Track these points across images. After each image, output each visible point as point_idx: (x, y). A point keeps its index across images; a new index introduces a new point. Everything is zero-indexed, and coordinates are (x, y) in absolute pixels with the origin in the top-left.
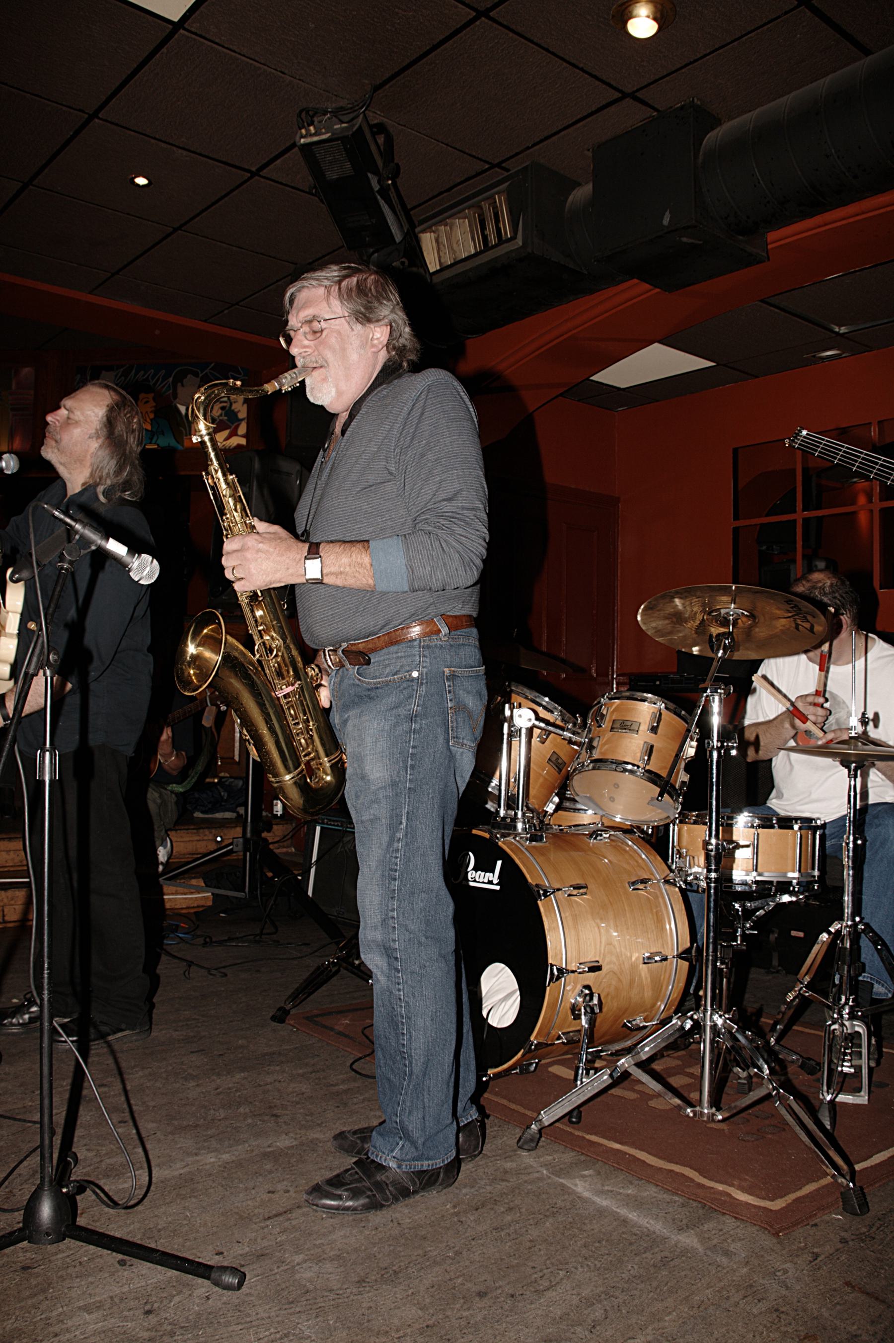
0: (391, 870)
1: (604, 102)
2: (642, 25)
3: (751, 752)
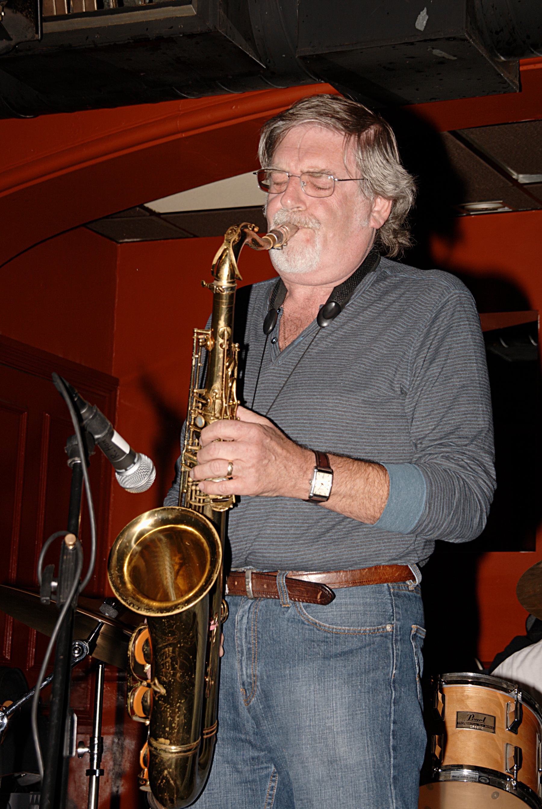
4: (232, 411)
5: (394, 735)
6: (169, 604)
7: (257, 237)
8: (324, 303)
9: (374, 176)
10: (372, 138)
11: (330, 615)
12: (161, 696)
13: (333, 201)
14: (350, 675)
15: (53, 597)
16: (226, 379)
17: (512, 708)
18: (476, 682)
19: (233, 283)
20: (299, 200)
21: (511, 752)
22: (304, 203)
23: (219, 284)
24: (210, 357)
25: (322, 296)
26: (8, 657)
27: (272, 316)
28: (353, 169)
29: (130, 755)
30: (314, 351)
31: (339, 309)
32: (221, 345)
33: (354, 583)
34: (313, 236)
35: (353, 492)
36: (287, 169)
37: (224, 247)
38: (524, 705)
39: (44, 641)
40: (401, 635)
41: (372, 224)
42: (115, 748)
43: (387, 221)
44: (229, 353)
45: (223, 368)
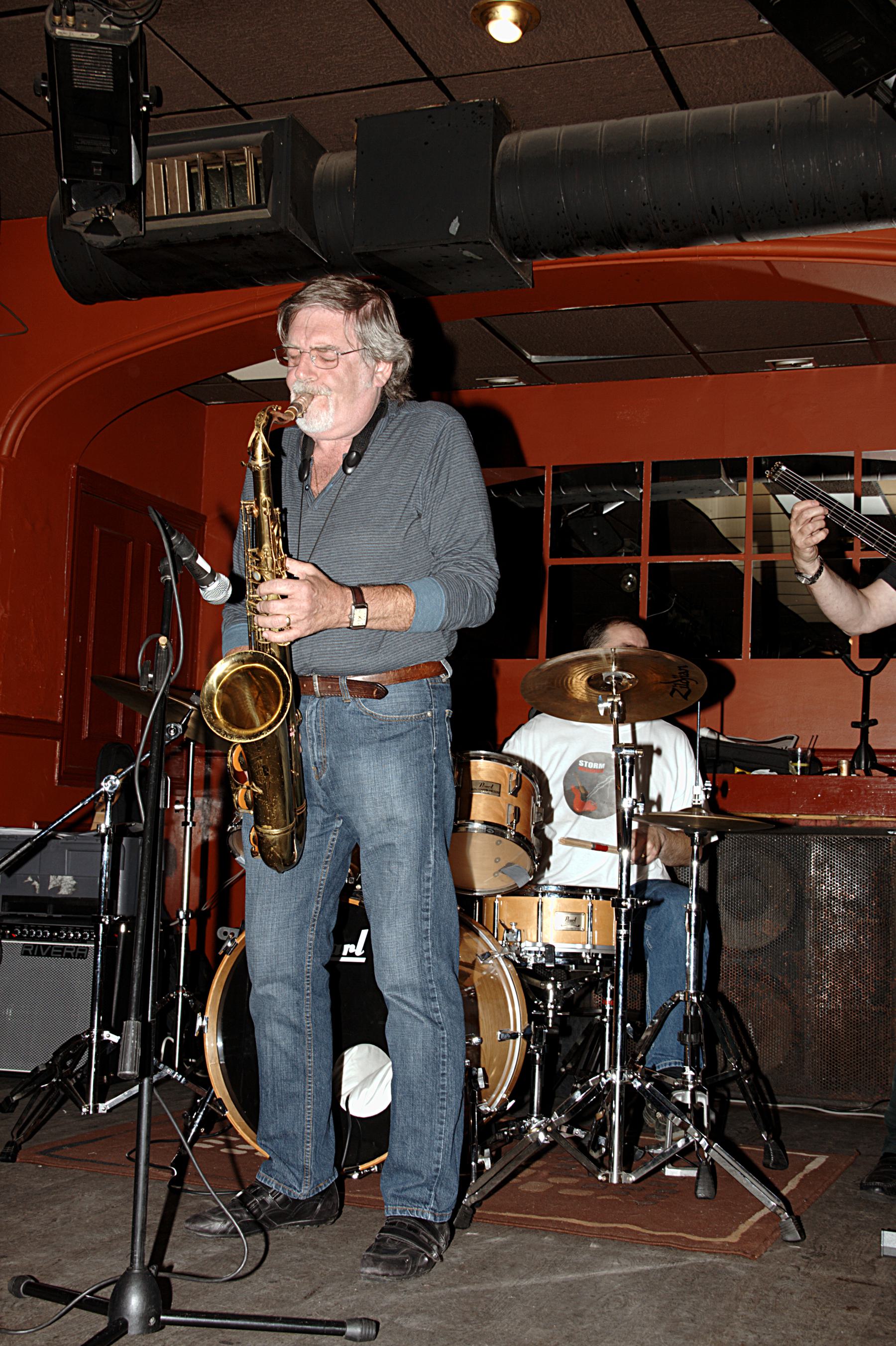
0: (423, 910)
1: (403, 78)
2: (504, 27)
3: (654, 809)
4: (282, 563)
5: (435, 797)
6: (256, 730)
7: (281, 415)
8: (347, 452)
9: (374, 345)
10: (370, 311)
11: (383, 707)
12: (259, 795)
13: (340, 370)
14: (402, 753)
15: (150, 686)
16: (273, 539)
17: (514, 778)
18: (487, 758)
19: (267, 460)
20: (310, 372)
21: (511, 810)
22: (316, 375)
23: (256, 463)
24: (257, 523)
25: (345, 447)
26: (120, 736)
27: (305, 465)
28: (354, 341)
29: (218, 812)
30: (343, 495)
31: (360, 457)
32: (265, 513)
33: (401, 680)
34: (327, 401)
35: (390, 609)
36: (298, 346)
37: (255, 432)
38: (523, 775)
39: (145, 720)
40: (437, 720)
41: (376, 384)
42: (205, 807)
43: (390, 379)
44: (273, 517)
45: (269, 529)
